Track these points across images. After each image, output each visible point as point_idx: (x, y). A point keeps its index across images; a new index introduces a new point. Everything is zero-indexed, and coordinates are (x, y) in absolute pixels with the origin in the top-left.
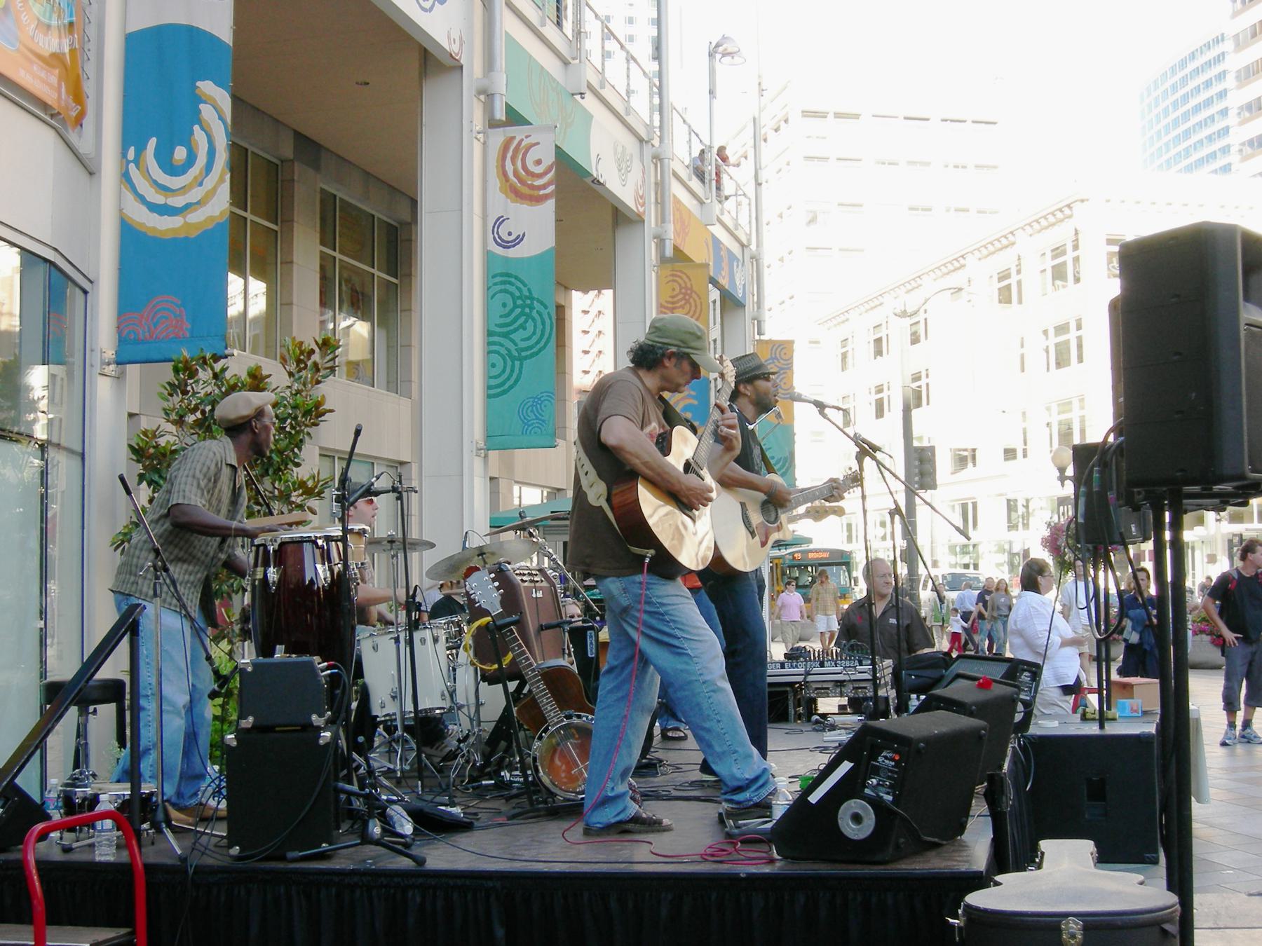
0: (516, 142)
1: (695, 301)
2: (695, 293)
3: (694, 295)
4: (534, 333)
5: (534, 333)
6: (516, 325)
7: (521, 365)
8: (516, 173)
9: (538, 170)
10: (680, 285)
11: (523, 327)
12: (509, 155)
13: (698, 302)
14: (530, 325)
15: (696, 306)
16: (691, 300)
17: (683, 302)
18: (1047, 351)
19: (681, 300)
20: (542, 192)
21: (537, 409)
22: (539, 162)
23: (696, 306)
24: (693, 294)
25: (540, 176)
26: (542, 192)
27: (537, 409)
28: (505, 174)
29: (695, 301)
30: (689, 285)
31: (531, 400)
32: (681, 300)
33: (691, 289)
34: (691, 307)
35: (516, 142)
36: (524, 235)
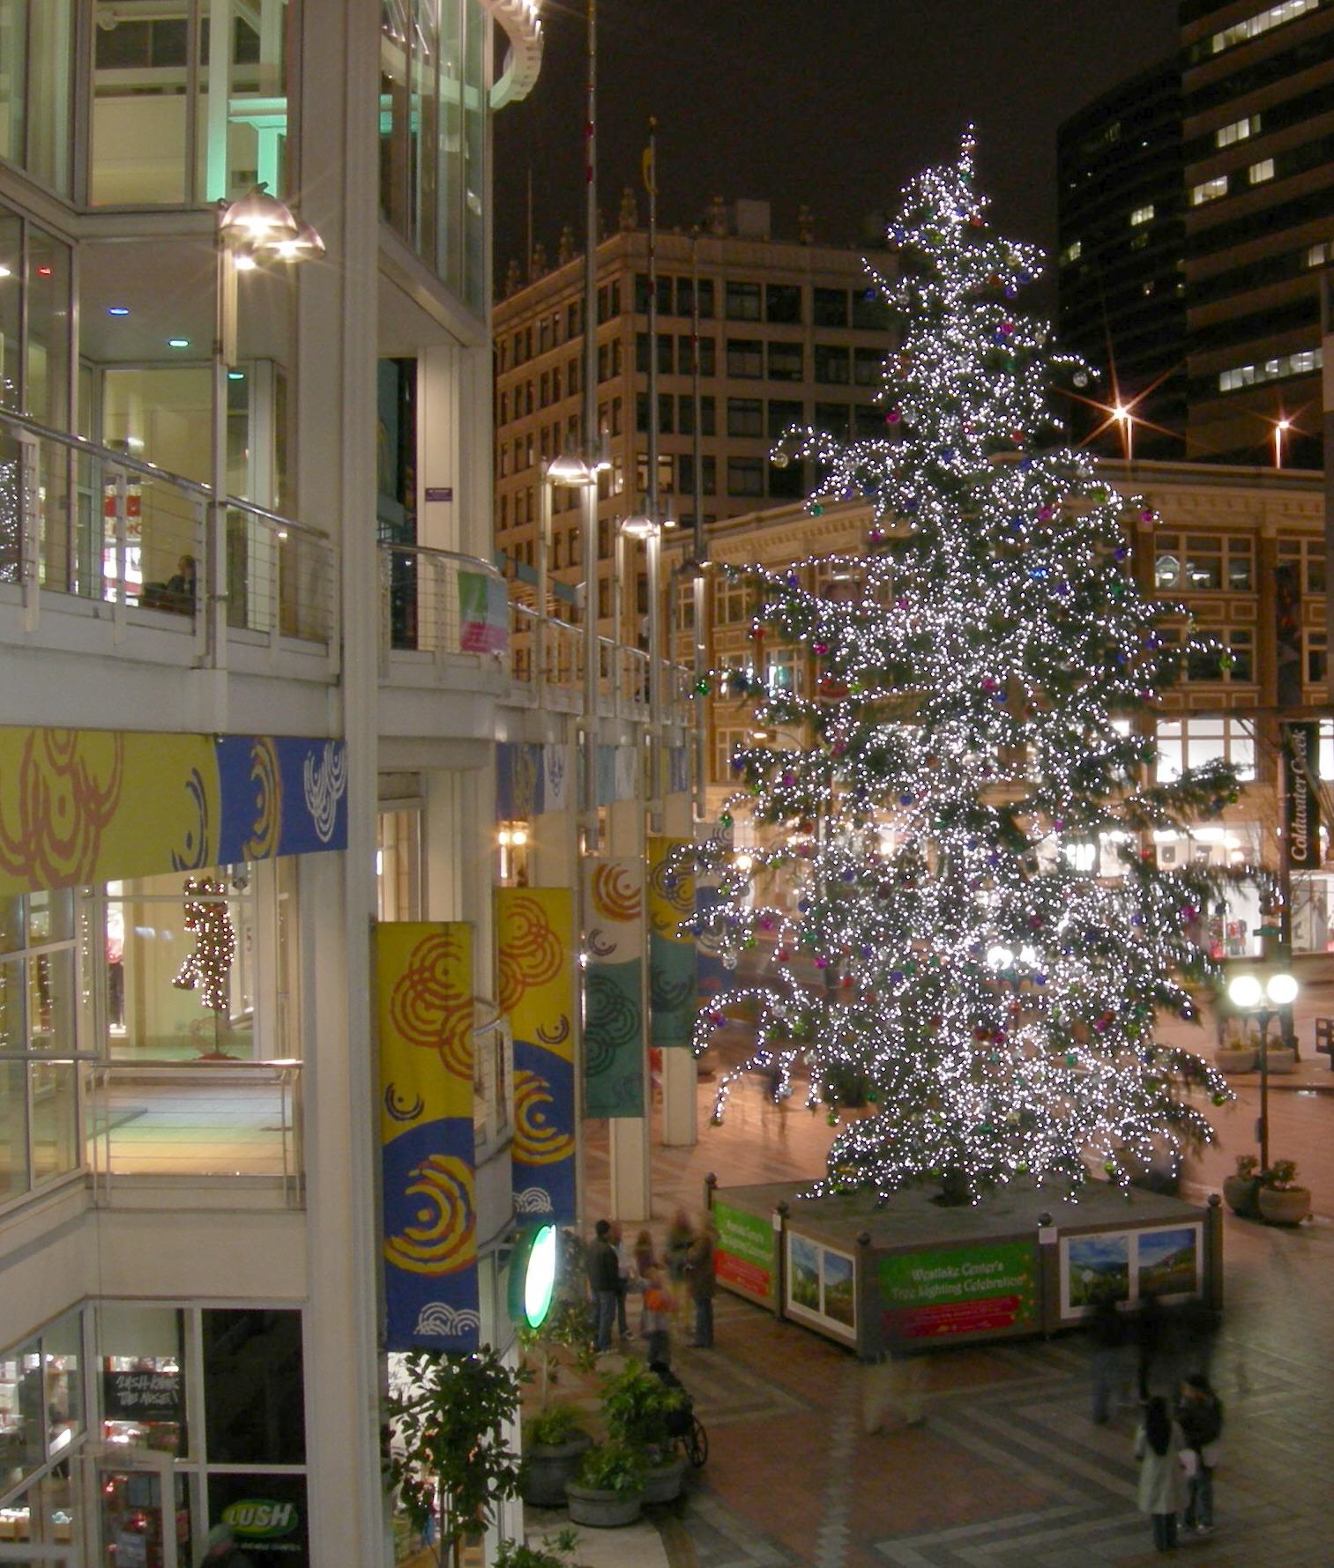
0: (606, 871)
1: (552, 947)
2: (553, 934)
3: (550, 937)
4: (541, 963)
5: (541, 963)
6: (525, 951)
7: (1274, 1072)
8: (608, 895)
9: (628, 893)
10: (528, 920)
11: (532, 954)
12: (602, 879)
13: (556, 947)
14: (539, 954)
15: (553, 955)
16: (546, 945)
17: (533, 947)
18: (198, 789)
19: (530, 943)
20: (631, 911)
21: (435, 993)
22: (627, 887)
23: (553, 955)
24: (550, 937)
25: (630, 898)
26: (631, 911)
27: (435, 993)
28: (598, 894)
29: (552, 947)
30: (543, 923)
31: (407, 984)
32: (530, 943)
33: (546, 928)
34: (545, 955)
35: (606, 871)
36: (195, 772)
